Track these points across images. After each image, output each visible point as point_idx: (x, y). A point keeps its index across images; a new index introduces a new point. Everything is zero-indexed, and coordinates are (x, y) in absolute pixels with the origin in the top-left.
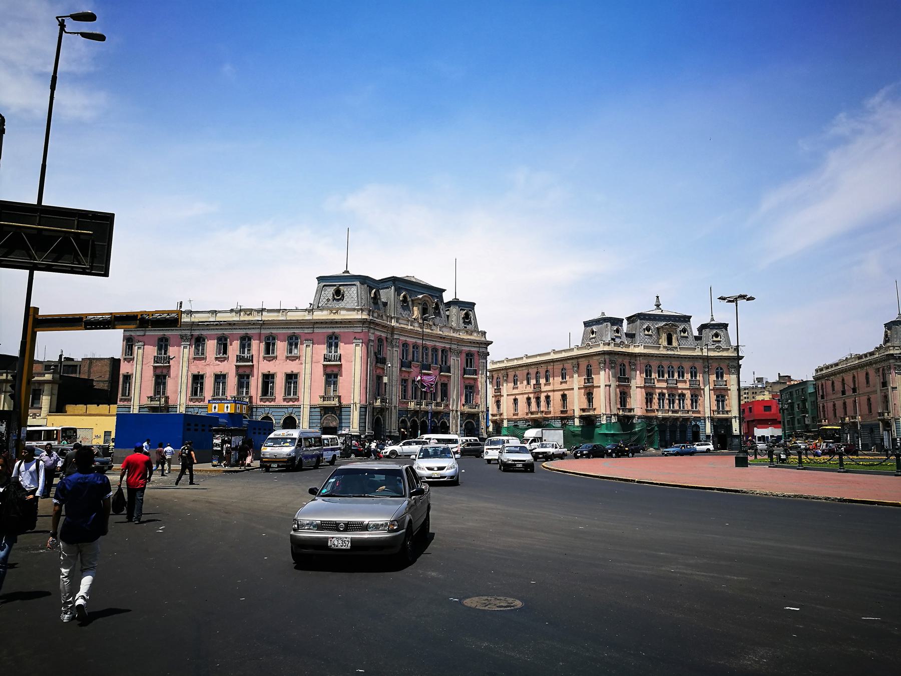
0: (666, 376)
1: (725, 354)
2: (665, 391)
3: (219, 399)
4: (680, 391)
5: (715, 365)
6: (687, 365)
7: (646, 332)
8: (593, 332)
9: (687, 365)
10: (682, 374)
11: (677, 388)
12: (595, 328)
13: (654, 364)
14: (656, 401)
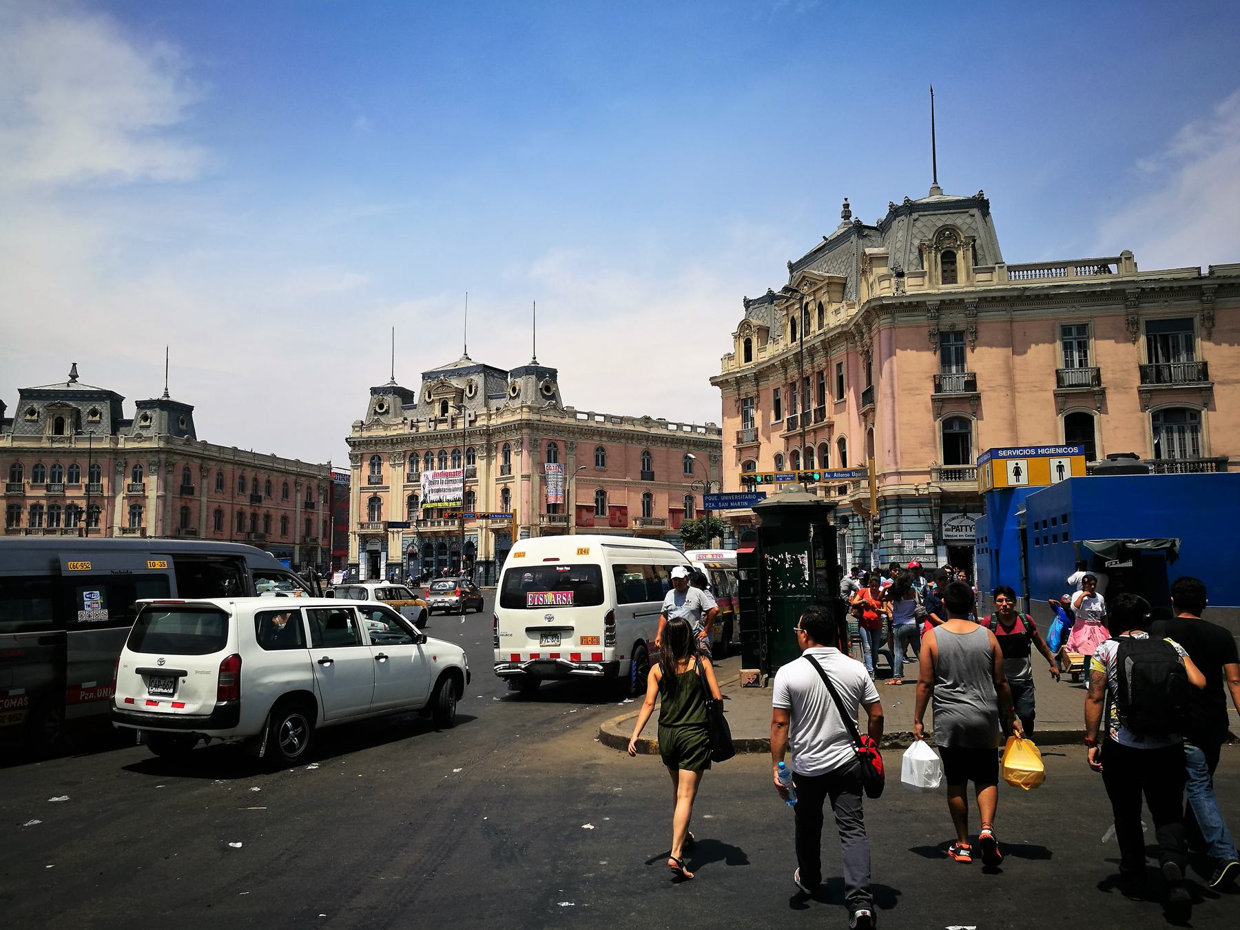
0: (47, 481)
1: (146, 445)
2: (43, 502)
3: (447, 475)
4: (69, 502)
5: (132, 462)
6: (84, 463)
7: (28, 417)
8: (32, 412)
9: (84, 463)
10: (74, 477)
11: (64, 497)
12: (37, 406)
13: (28, 463)
14: (25, 516)
